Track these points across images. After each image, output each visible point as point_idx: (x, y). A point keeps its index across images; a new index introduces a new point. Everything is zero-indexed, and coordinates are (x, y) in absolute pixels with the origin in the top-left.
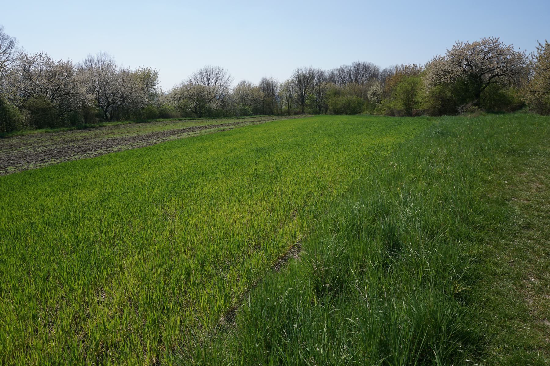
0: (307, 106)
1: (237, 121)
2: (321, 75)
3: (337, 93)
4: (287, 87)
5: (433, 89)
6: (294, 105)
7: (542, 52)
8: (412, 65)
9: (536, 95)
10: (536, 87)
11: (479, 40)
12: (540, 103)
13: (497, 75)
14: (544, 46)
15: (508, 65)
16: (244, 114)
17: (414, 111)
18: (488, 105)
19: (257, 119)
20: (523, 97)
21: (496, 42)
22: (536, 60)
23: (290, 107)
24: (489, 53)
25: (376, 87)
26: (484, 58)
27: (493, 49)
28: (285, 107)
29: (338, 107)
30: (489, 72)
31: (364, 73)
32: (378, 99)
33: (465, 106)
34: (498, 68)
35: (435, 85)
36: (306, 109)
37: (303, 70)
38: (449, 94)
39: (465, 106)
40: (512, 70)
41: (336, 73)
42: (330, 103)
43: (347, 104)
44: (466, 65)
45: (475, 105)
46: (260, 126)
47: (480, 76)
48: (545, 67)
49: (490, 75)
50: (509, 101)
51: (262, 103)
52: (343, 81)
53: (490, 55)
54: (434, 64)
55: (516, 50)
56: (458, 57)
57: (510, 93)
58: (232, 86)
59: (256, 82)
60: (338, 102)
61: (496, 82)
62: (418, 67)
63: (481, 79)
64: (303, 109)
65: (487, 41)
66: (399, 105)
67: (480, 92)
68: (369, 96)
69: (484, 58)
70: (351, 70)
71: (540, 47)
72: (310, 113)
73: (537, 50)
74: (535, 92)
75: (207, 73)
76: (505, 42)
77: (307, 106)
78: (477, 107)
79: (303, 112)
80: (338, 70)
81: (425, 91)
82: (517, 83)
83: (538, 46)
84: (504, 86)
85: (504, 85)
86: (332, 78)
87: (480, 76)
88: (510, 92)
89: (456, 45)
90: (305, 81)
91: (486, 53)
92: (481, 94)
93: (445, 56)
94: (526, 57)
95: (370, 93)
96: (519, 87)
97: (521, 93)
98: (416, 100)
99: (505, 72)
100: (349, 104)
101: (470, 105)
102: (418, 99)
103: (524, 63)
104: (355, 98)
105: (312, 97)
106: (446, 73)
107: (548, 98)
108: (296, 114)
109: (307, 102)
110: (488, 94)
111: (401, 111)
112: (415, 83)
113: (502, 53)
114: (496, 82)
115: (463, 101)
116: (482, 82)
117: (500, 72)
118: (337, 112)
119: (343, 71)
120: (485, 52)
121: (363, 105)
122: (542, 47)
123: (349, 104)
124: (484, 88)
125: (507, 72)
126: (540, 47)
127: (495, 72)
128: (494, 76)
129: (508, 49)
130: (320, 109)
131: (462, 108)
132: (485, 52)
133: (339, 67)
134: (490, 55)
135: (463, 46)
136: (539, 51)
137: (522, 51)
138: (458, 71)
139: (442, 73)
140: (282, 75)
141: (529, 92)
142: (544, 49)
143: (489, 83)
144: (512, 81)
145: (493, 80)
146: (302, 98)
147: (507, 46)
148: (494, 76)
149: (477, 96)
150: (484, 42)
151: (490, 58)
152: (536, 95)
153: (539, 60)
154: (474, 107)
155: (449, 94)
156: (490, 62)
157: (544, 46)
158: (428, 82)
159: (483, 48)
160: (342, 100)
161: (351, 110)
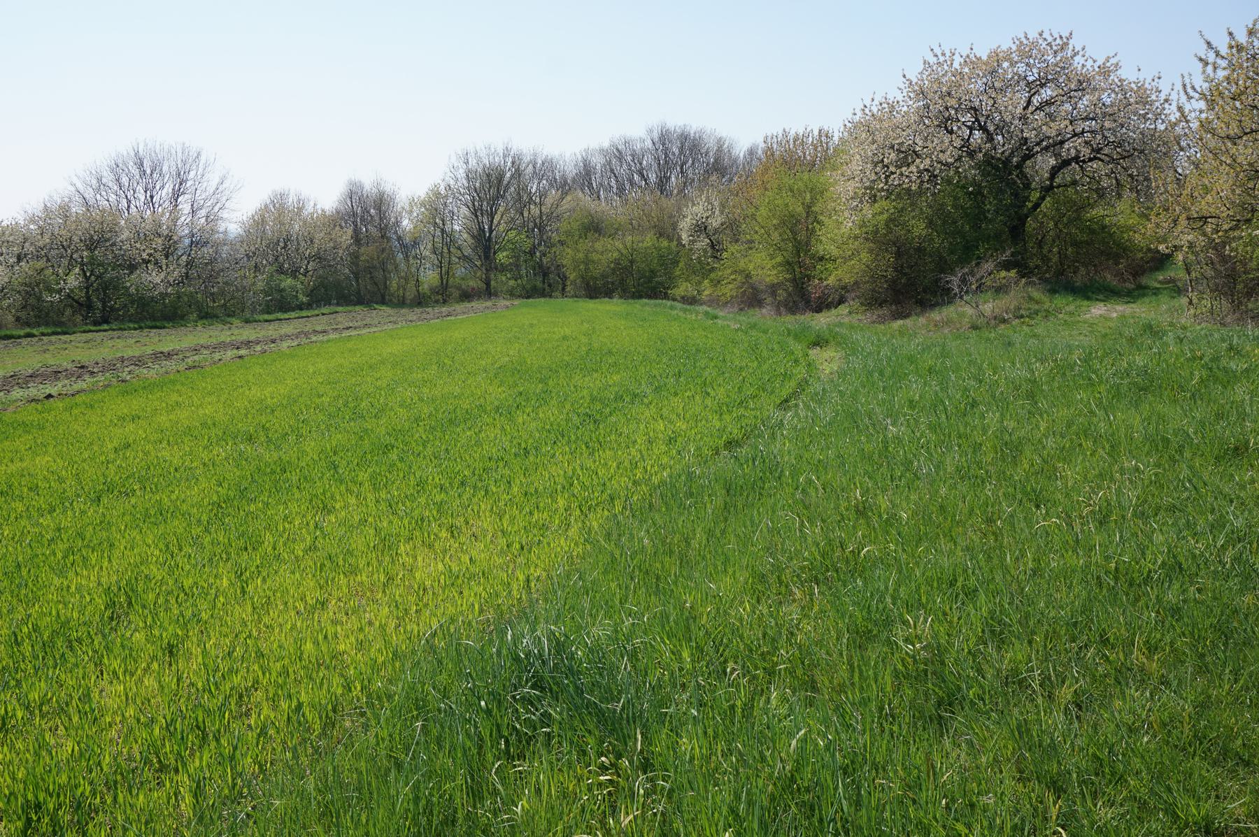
0: (503, 269)
1: (248, 333)
2: (545, 170)
3: (594, 227)
4: (435, 208)
5: (868, 212)
6: (460, 271)
7: (1221, 74)
8: (816, 133)
9: (1208, 229)
10: (1204, 205)
11: (1006, 44)
12: (1224, 259)
13: (1076, 159)
14: (1224, 51)
15: (1107, 124)
16: (280, 304)
17: (814, 289)
18: (1055, 259)
19: (318, 321)
20: (1165, 240)
21: (1064, 47)
22: (1202, 105)
23: (445, 276)
24: (1042, 85)
25: (699, 208)
26: (1029, 102)
27: (1052, 75)
28: (430, 277)
29: (596, 273)
30: (1046, 148)
31: (683, 160)
32: (713, 246)
33: (972, 273)
34: (1075, 135)
35: (874, 199)
36: (502, 281)
37: (483, 154)
38: (919, 229)
39: (972, 273)
40: (1127, 148)
41: (598, 161)
42: (568, 257)
43: (625, 263)
44: (971, 129)
45: (1007, 266)
46: (292, 356)
47: (1019, 166)
48: (1234, 130)
49: (1052, 162)
50: (1119, 245)
51: (346, 269)
52: (621, 189)
53: (1047, 93)
54: (865, 128)
55: (1128, 73)
56: (943, 104)
57: (1121, 220)
58: (235, 218)
59: (324, 195)
60: (595, 257)
61: (1074, 183)
62: (836, 139)
63: (1023, 175)
64: (488, 284)
65: (1034, 44)
66: (765, 267)
67: (1023, 220)
68: (684, 236)
69: (1029, 102)
70: (644, 152)
71: (1211, 57)
72: (512, 294)
73: (1200, 65)
74: (1204, 219)
75: (145, 169)
76: (1091, 50)
77: (503, 269)
78: (1013, 273)
79: (488, 292)
80: (602, 151)
81: (845, 224)
82: (1141, 187)
83: (1202, 51)
84: (1101, 196)
85: (1101, 192)
86: (586, 174)
87: (1019, 166)
88: (1120, 213)
89: (933, 60)
90: (494, 187)
91: (1034, 87)
92: (1031, 223)
93: (900, 98)
94: (1163, 97)
95: (685, 225)
96: (1149, 197)
97: (1158, 225)
98: (820, 249)
99: (1099, 151)
100: (632, 262)
101: (988, 266)
102: (826, 244)
103: (1157, 116)
104: (649, 240)
105: (520, 243)
106: (907, 156)
107: (1253, 242)
108: (466, 296)
109: (502, 257)
110: (1051, 224)
111: (779, 285)
112: (818, 192)
113: (1083, 85)
114: (1074, 183)
115: (967, 252)
116: (1027, 186)
117: (1086, 152)
118: (595, 289)
119: (620, 156)
120: (1028, 84)
121: (676, 263)
122: (1217, 54)
123: (632, 262)
124: (1037, 206)
125: (1106, 151)
126: (1211, 57)
127: (1069, 149)
128: (1066, 163)
129: (1105, 72)
130: (543, 281)
131: (963, 281)
132: (1028, 84)
133: (606, 145)
134: (1047, 93)
135: (956, 65)
136: (1210, 69)
137: (1146, 76)
138: (944, 148)
139: (893, 156)
140: (416, 167)
141: (1183, 221)
142: (1223, 63)
143: (1051, 187)
144: (1123, 178)
145: (1065, 176)
146: (485, 243)
147: (1100, 62)
148: (1066, 163)
149: (1016, 231)
150: (1026, 51)
151: (1048, 103)
152: (1208, 229)
153: (1211, 104)
154: (1003, 274)
155: (919, 229)
156: (1050, 115)
157: (1224, 51)
158: (851, 186)
159: (1021, 68)
160: (606, 251)
161: (641, 281)
